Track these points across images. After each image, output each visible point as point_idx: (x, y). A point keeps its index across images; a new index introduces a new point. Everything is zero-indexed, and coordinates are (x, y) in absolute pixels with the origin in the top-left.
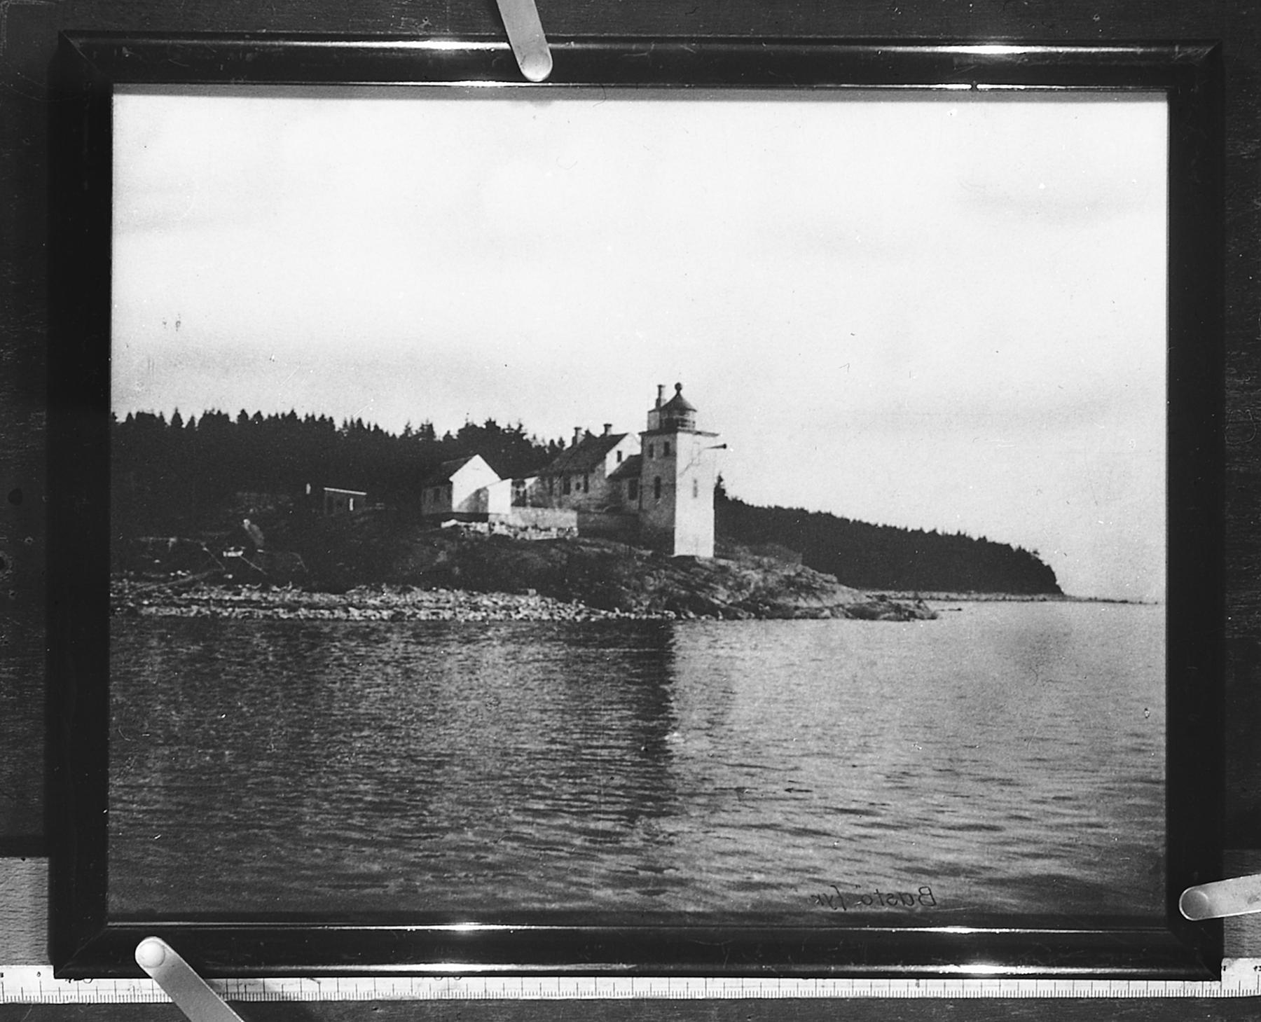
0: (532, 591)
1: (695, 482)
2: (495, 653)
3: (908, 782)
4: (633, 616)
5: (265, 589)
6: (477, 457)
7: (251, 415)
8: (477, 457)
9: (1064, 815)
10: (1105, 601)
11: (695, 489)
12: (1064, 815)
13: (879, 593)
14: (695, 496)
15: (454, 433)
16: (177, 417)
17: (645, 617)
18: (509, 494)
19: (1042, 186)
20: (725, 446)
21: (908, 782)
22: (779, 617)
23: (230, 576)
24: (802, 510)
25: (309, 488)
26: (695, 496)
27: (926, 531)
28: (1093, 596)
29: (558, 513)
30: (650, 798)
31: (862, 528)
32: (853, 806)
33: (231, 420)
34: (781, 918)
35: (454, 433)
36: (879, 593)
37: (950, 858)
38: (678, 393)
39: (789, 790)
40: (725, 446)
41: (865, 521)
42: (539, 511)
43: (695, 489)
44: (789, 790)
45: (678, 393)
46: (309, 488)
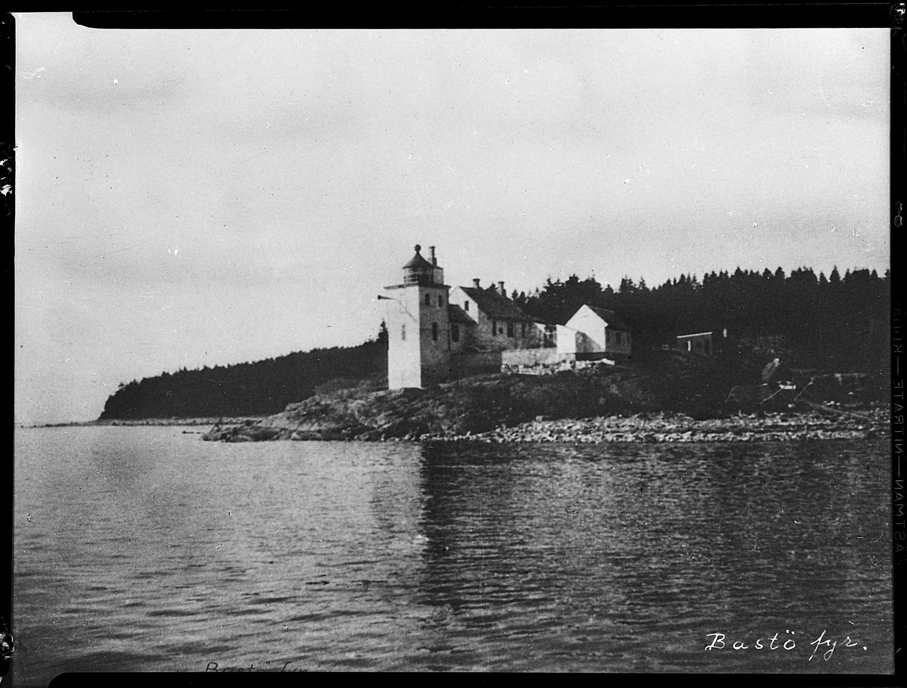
0: (539, 418)
1: (404, 327)
2: (570, 469)
3: (227, 575)
4: (446, 439)
5: (761, 416)
6: (585, 306)
7: (773, 272)
8: (585, 306)
9: (98, 603)
10: (58, 425)
11: (404, 333)
12: (98, 603)
13: (245, 419)
14: (404, 338)
15: (657, 288)
16: (835, 273)
17: (456, 438)
18: (559, 337)
19: (116, 81)
20: (380, 297)
21: (227, 575)
22: (334, 439)
23: (790, 406)
24: (315, 350)
25: (725, 332)
26: (404, 338)
27: (171, 373)
28: (74, 421)
29: (518, 353)
30: (442, 590)
31: (242, 369)
32: (272, 596)
33: (879, 276)
34: (540, 558)
35: (657, 288)
36: (245, 419)
37: (192, 638)
38: (418, 254)
39: (326, 583)
40: (380, 297)
41: (263, 359)
42: (533, 351)
43: (404, 333)
44: (326, 583)
45: (418, 254)
46: (725, 332)
